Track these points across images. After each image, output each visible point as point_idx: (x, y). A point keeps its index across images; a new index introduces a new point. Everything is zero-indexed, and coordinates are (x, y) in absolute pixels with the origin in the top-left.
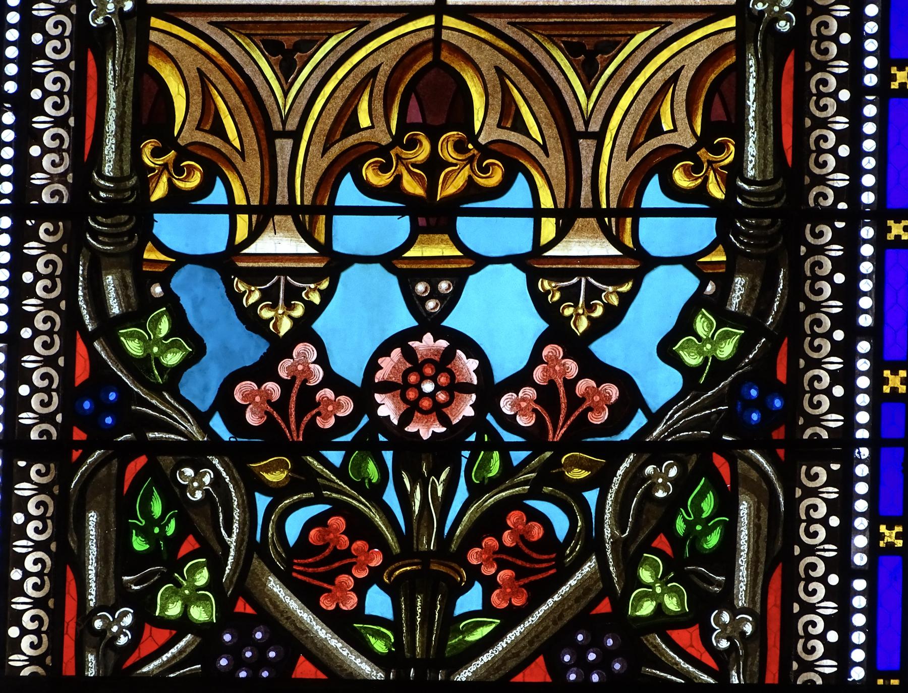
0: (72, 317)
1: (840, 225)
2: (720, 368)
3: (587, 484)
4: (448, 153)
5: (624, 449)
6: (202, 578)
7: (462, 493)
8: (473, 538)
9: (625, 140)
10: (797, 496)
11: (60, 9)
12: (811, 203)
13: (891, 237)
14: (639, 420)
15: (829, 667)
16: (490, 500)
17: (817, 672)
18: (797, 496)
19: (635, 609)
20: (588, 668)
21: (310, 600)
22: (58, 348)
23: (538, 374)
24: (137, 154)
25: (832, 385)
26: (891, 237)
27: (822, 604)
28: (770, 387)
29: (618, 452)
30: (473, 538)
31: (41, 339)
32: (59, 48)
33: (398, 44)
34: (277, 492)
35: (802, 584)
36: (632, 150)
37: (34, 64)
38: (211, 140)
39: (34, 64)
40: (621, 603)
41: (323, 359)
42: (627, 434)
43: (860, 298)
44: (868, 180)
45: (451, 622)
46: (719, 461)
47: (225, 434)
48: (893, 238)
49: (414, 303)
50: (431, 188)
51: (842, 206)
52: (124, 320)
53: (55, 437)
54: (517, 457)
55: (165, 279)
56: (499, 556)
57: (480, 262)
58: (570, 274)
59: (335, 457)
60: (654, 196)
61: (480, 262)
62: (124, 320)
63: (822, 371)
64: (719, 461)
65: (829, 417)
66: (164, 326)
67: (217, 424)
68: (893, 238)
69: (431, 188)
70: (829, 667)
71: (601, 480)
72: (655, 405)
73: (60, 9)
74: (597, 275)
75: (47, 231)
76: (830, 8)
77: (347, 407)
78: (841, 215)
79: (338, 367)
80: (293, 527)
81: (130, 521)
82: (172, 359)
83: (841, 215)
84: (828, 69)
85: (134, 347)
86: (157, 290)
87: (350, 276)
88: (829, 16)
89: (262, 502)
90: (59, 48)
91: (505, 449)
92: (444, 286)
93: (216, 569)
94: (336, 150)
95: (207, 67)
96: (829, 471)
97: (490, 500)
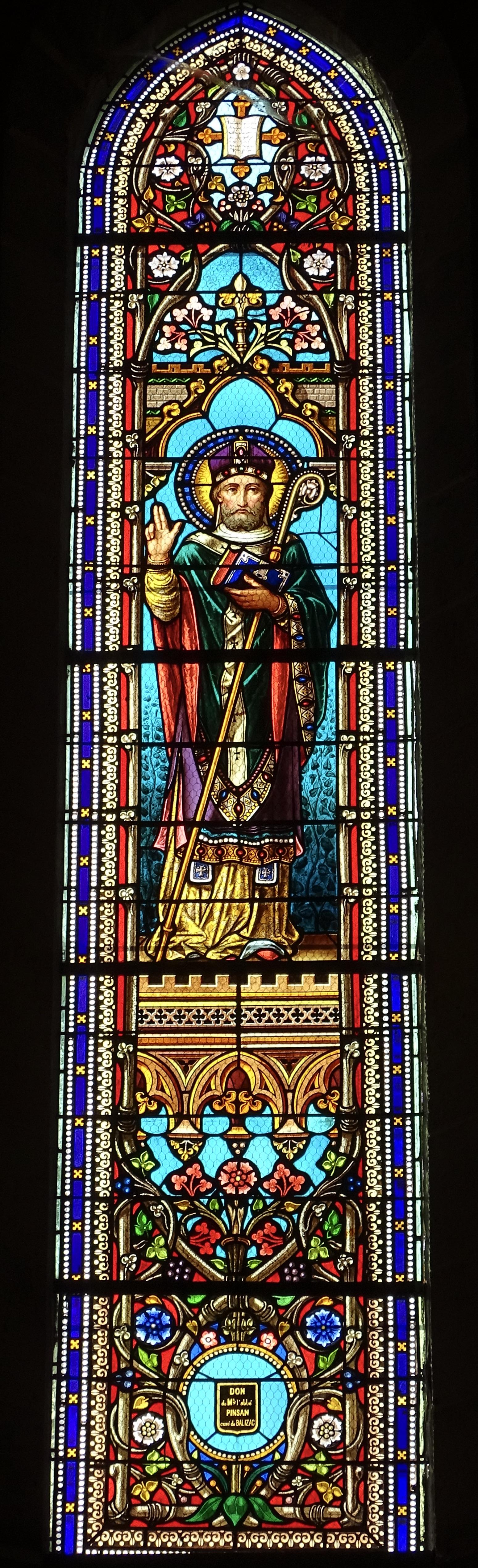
0: (114, 1154)
2: (339, 1170)
3: (294, 1212)
4: (242, 1098)
5: (306, 1199)
6: (162, 1242)
7: (250, 1215)
8: (254, 1231)
9: (303, 1090)
14: (311, 1189)
15: (373, 642)
16: (260, 1217)
20: (293, 1276)
21: (196, 1250)
23: (276, 1176)
24: (135, 1097)
28: (357, 1179)
29: (305, 1200)
30: (254, 1231)
34: (184, 1213)
36: (305, 1092)
38: (159, 1093)
40: (306, 1254)
41: (202, 1169)
42: (307, 1194)
45: (246, 1260)
46: (338, 1204)
47: (168, 1193)
49: (232, 1151)
50: (237, 1110)
52: (133, 1154)
54: (268, 1201)
55: (145, 1142)
57: (254, 1135)
58: (283, 1139)
59: (205, 1201)
60: (312, 1110)
61: (254, 1135)
62: (132, 1155)
64: (338, 1204)
66: (146, 1157)
67: (164, 1189)
69: (237, 1110)
70: (373, 642)
71: (298, 1211)
72: (316, 1184)
74: (296, 1139)
77: (209, 1185)
79: (207, 1171)
80: (190, 1225)
82: (149, 1168)
85: (136, 1165)
86: (143, 1144)
87: (211, 1141)
89: (179, 1215)
91: (264, 1199)
92: (242, 1145)
93: (166, 1239)
94: (204, 1097)
95: (159, 1069)
97: (260, 1217)
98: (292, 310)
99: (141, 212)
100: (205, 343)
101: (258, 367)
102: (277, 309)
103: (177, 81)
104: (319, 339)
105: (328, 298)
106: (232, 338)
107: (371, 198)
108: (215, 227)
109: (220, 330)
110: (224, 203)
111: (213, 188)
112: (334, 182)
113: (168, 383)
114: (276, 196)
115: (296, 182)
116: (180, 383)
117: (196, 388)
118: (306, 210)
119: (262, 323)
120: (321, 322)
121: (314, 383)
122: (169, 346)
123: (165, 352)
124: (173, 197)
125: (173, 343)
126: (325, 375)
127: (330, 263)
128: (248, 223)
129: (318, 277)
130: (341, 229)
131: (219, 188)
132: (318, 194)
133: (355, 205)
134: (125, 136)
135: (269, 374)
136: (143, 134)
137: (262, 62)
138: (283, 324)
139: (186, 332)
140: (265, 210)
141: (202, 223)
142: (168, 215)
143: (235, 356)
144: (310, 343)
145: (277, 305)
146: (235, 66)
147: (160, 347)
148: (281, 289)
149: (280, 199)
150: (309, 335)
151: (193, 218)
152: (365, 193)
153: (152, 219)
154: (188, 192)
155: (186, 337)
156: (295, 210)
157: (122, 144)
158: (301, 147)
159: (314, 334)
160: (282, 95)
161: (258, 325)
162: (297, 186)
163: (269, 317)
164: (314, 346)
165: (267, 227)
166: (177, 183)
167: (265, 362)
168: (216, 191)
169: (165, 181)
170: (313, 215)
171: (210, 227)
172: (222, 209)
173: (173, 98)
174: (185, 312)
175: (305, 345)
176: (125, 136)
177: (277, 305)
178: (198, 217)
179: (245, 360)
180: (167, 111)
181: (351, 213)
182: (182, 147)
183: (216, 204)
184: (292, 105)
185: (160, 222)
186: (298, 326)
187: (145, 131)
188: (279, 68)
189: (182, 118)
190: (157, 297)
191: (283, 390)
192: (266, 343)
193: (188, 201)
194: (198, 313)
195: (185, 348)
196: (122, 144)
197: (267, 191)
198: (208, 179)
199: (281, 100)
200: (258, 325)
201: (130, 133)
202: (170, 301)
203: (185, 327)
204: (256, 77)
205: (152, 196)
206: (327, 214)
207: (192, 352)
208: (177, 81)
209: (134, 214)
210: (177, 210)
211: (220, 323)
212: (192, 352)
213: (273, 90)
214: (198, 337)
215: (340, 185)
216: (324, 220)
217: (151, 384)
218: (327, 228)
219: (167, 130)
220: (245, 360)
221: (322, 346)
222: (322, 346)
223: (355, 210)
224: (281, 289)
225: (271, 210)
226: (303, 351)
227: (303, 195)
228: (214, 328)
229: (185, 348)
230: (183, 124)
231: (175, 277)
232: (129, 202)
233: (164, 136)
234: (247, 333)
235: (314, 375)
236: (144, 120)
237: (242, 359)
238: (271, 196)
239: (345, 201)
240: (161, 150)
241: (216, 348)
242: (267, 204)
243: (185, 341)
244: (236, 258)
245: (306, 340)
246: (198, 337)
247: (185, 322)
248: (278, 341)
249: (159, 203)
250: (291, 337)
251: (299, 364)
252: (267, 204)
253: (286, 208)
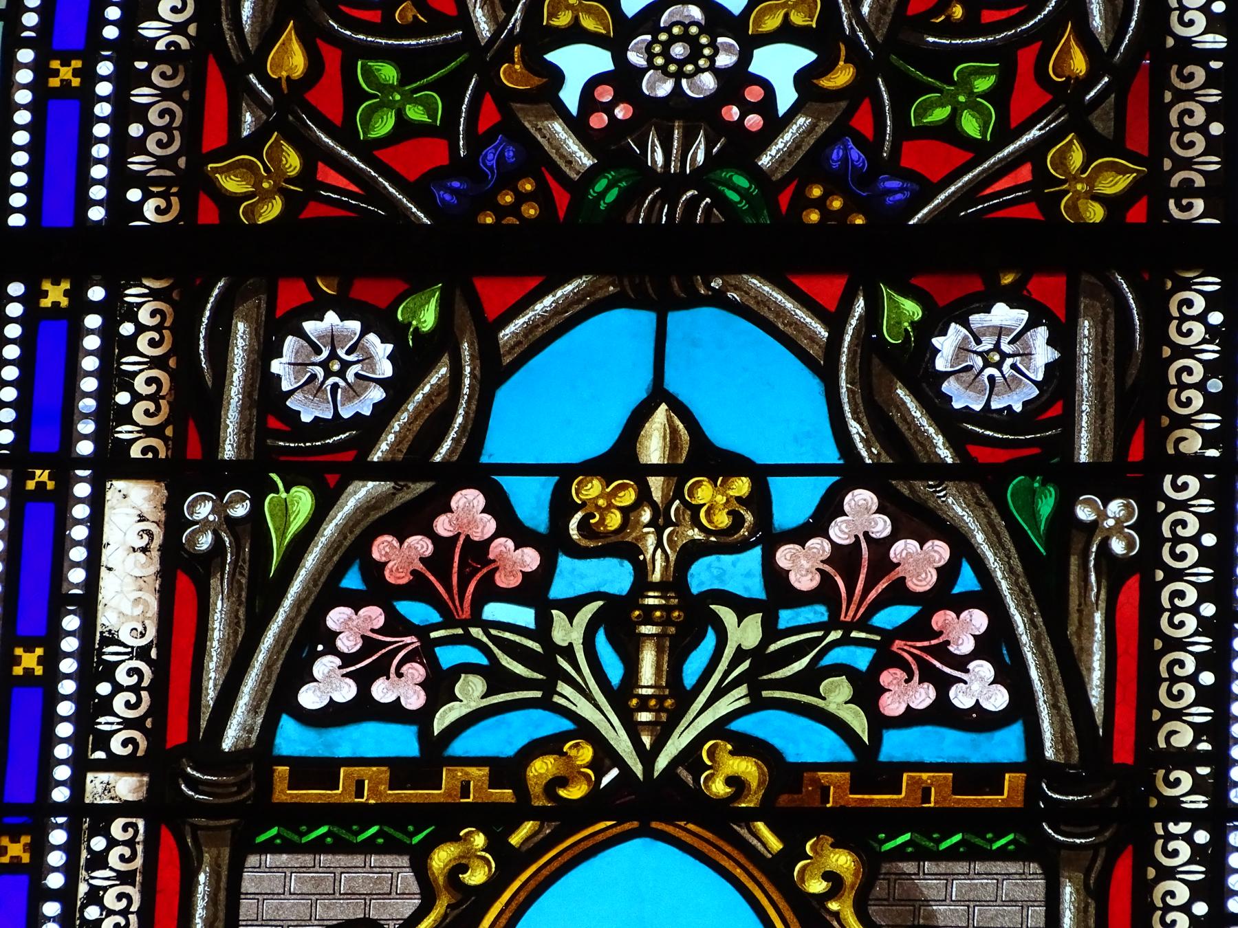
1: (1203, 771)
12: (1162, 745)
17: (1185, 722)
25: (1205, 379)
27: (1195, 570)
32: (165, 141)
33: (279, 916)
35: (1160, 842)
37: (129, 160)
39: (129, 160)
43: (1228, 898)
51: (1204, 746)
56: (864, 545)
63: (1193, 172)
65: (1194, 710)
76: (1196, 93)
78: (1204, 759)
81: (638, 152)
83: (1204, 759)
84: (1185, 578)
88: (1179, 723)
90: (165, 141)
98: (881, 547)
100: (497, 679)
101: (719, 788)
102: (815, 543)
104: (983, 669)
105: (1029, 502)
106: (615, 671)
108: (562, 199)
109: (566, 632)
110: (605, 94)
111: (564, 20)
113: (341, 847)
116: (392, 847)
117: (459, 868)
118: (950, 130)
119: (743, 607)
120: (988, 599)
121: (952, 855)
122: (346, 692)
123: (333, 716)
124: (388, 73)
125: (364, 680)
126: (998, 820)
127: (1043, 353)
128: (702, 178)
129: (987, 416)
130: (1096, 213)
131: (588, 23)
135: (765, 812)
138: (834, 611)
139: (422, 631)
140: (775, 125)
141: (508, 180)
142: (367, 149)
143: (621, 742)
144: (943, 684)
145: (818, 525)
147: (310, 698)
148: (831, 456)
149: (842, 77)
150: (942, 652)
151: (467, 168)
152: (1203, 57)
153: (293, 161)
154: (447, 51)
155: (425, 654)
156: (903, 131)
159: (965, 646)
161: (727, 615)
163: (774, 577)
164: (961, 698)
165: (784, 199)
167: (746, 767)
168: (575, 35)
170: (981, 150)
171: (542, 196)
172: (599, 121)
174: (421, 545)
175: (923, 697)
177: (818, 525)
178: (490, 156)
179: (662, 762)
181: (1138, 140)
186: (894, 616)
190: (302, 501)
191: (816, 886)
192: (753, 693)
194: (477, 551)
195: (414, 700)
197: (787, 34)
200: (727, 615)
202: (365, 509)
203: (417, 612)
205: (297, 62)
206: (1035, 152)
207: (444, 718)
209: (214, 137)
211: (571, 607)
212: (444, 718)
214: (474, 656)
216: (1025, 173)
217: (269, 848)
218: (1031, 212)
220: (662, 762)
221: (998, 699)
222: (998, 699)
223: (1160, 130)
224: (831, 456)
226: (911, 718)
227: (941, 63)
228: (544, 622)
229: (414, 700)
231: (384, 412)
232: (196, 82)
234: (676, 651)
235: (947, 820)
237: (648, 758)
238: (806, 56)
241: (547, 704)
243: (416, 671)
244: (645, 320)
245: (929, 675)
246: (474, 656)
247: (417, 589)
248: (810, 681)
249: (327, 97)
250: (861, 658)
251: (890, 775)
252: (786, 97)
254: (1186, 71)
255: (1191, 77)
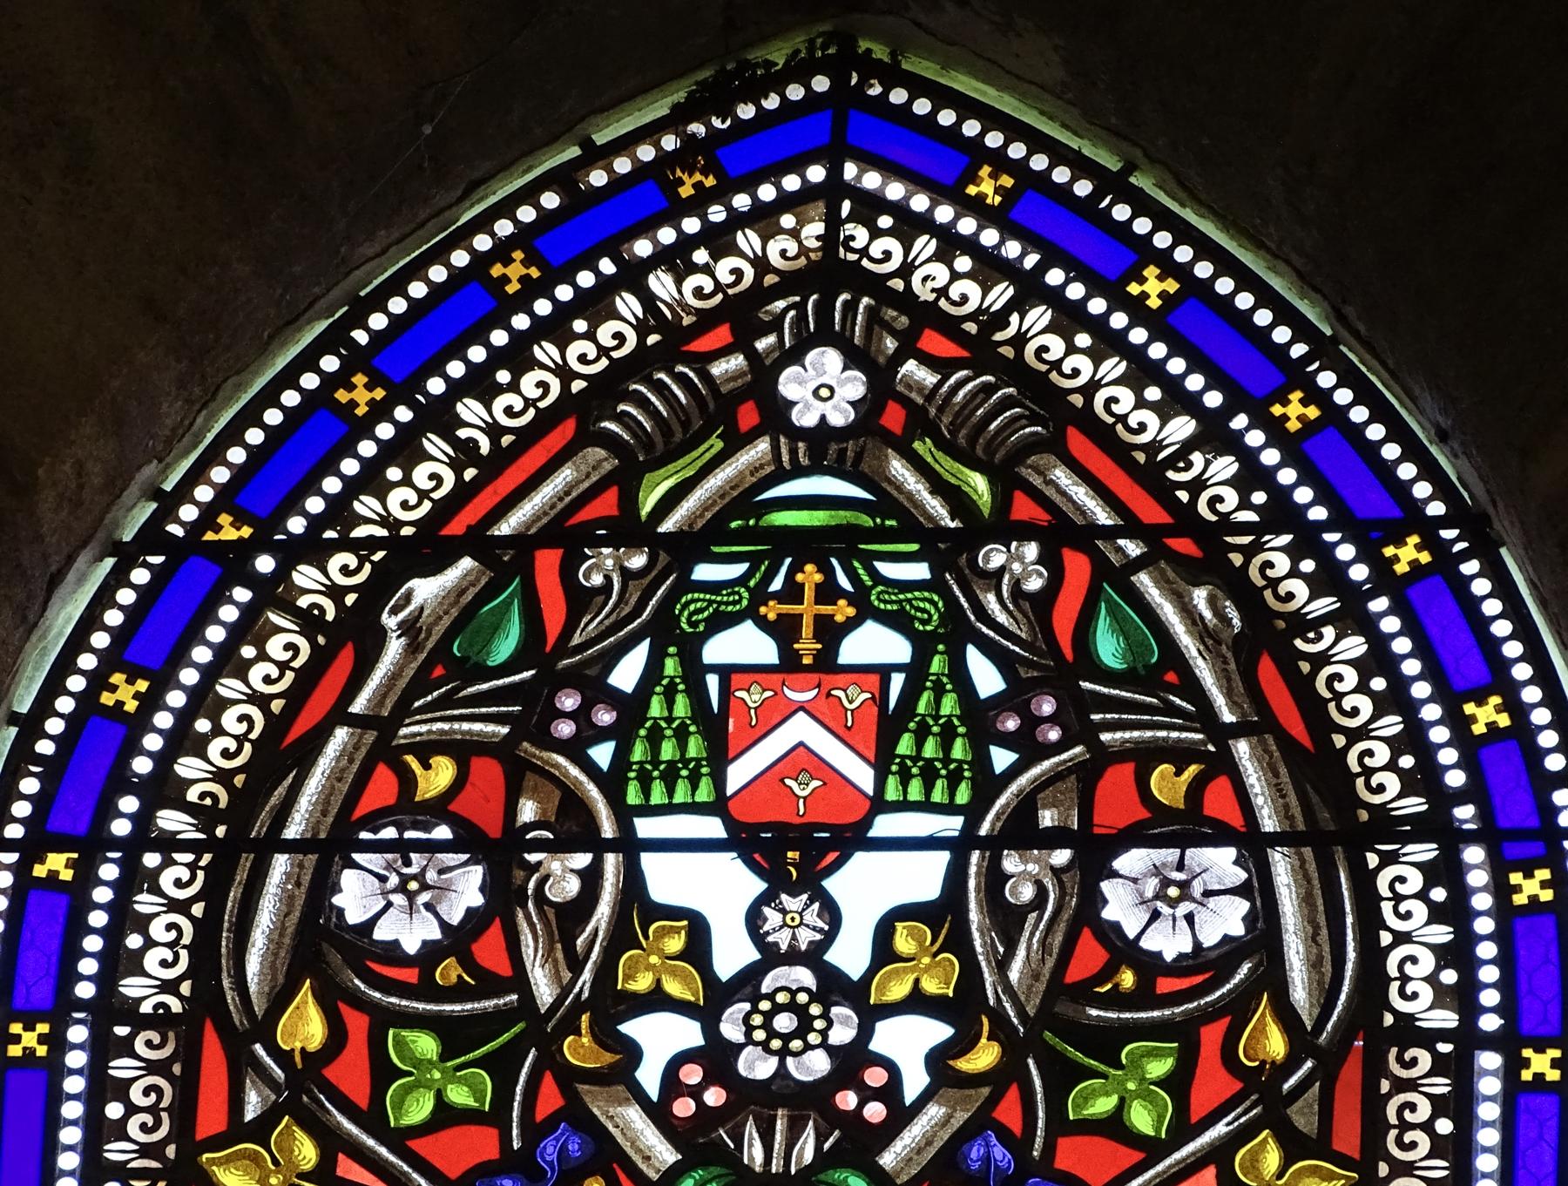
10: (202, 904)
11: (1407, 1169)
13: (1479, 729)
18: (202, 904)
19: (629, 977)
22: (165, 1133)
26: (1479, 729)
31: (138, 1119)
44: (1411, 667)
48: (1484, 730)
53: (223, 804)
68: (1484, 730)
73: (1407, 1169)
75: (149, 1044)
96: (1436, 1056)
99: (253, 1104)
103: (494, 430)
107: (1459, 1069)
110: (692, 1074)
111: (642, 983)
112: (1273, 979)
114: (962, 1043)
115: (1076, 972)
124: (426, 1044)
131: (673, 988)
132: (1184, 1035)
133: (1373, 1106)
134: (204, 700)
136: (297, 696)
137: (933, 342)
140: (901, 1116)
142: (398, 1139)
146: (795, 355)
152: (1428, 1039)
156: (1060, 1125)
157: (182, 740)
158: (1117, 782)
160: (1023, 508)
162: (1084, 992)
166: (449, 971)
168: (657, 1000)
169: (392, 951)
172: (684, 1108)
173: (456, 527)
176: (204, 700)
180: (425, 590)
181: (1347, 1138)
182: (488, 772)
183: (649, 1077)
184: (1077, 566)
185: (347, 1168)
187: (308, 678)
188: (1016, 371)
189: (496, 627)
193: (502, 1067)
196: (182, 740)
197: (918, 1003)
198: (622, 937)
199: (1025, 532)
201: (229, 687)
204: (894, 417)
206: (1221, 1155)
208: (494, 430)
209: (211, 1119)
210: (446, 1114)
213: (979, 485)
215: (1300, 994)
219: (420, 684)
223: (1374, 1124)
225: (934, 1111)
227: (1107, 1044)
230: (505, 647)
232: (190, 1053)
233: (403, 711)
236: (309, 622)
238: (940, 1032)
239: (1327, 1074)
240: (382, 788)
242: (915, 1082)
249: (351, 1073)
252: (915, 1082)
253: (1009, 1112)
254: (1408, 1056)
255: (1414, 1062)
